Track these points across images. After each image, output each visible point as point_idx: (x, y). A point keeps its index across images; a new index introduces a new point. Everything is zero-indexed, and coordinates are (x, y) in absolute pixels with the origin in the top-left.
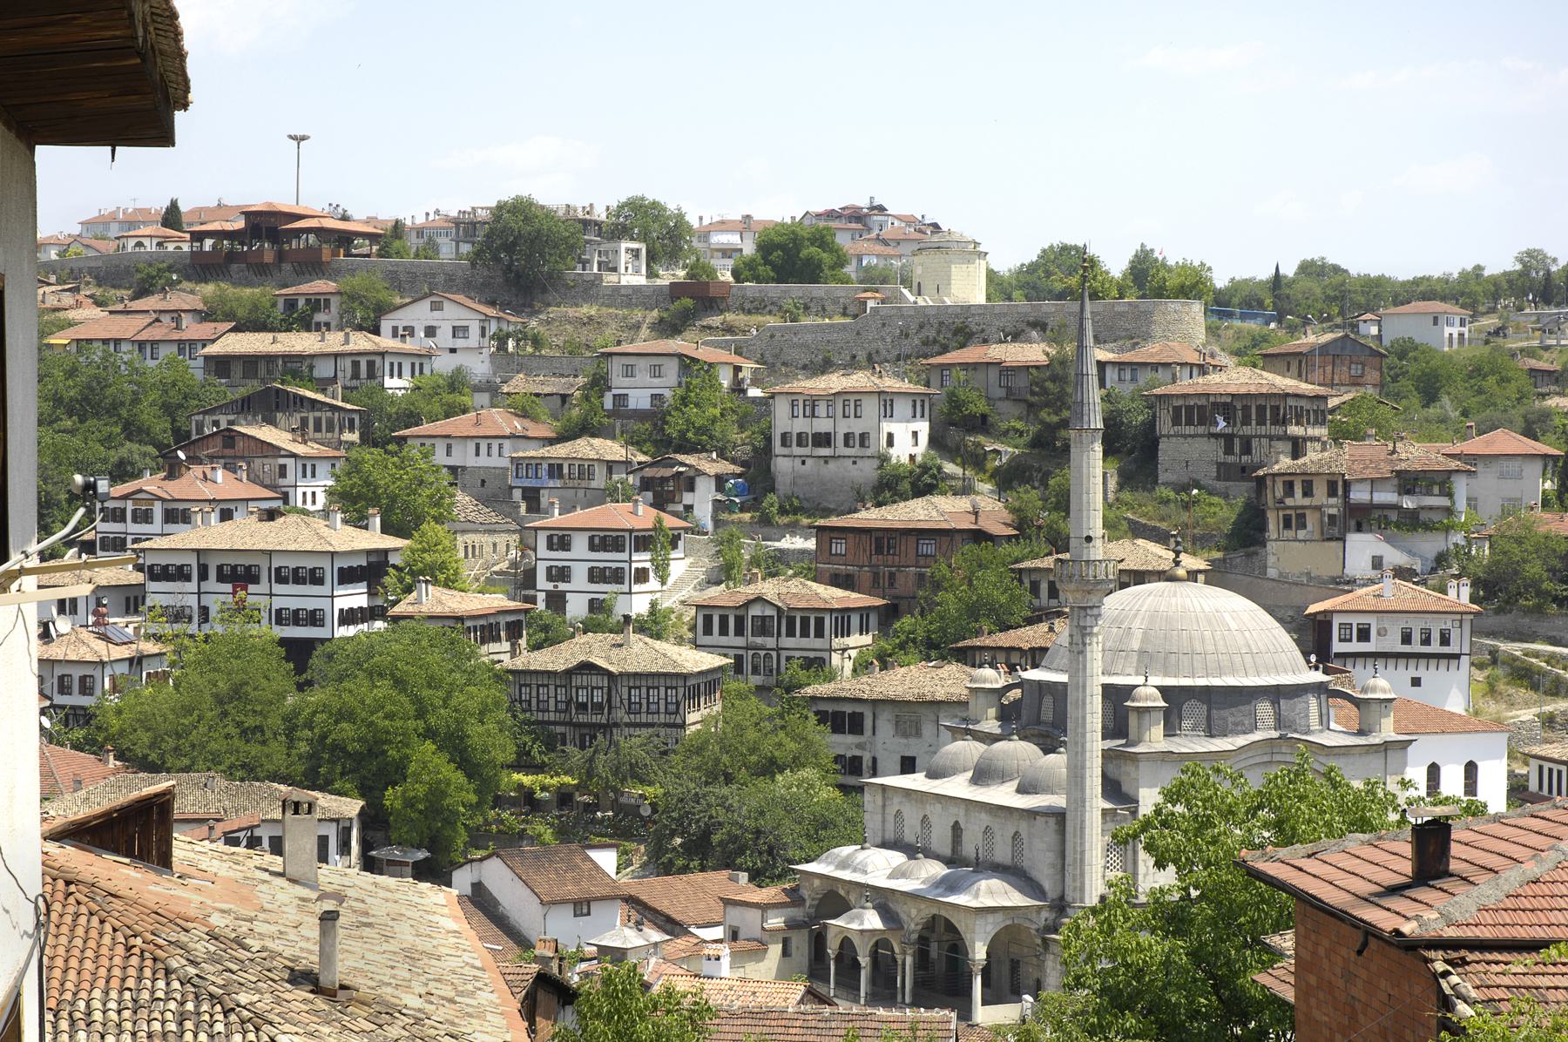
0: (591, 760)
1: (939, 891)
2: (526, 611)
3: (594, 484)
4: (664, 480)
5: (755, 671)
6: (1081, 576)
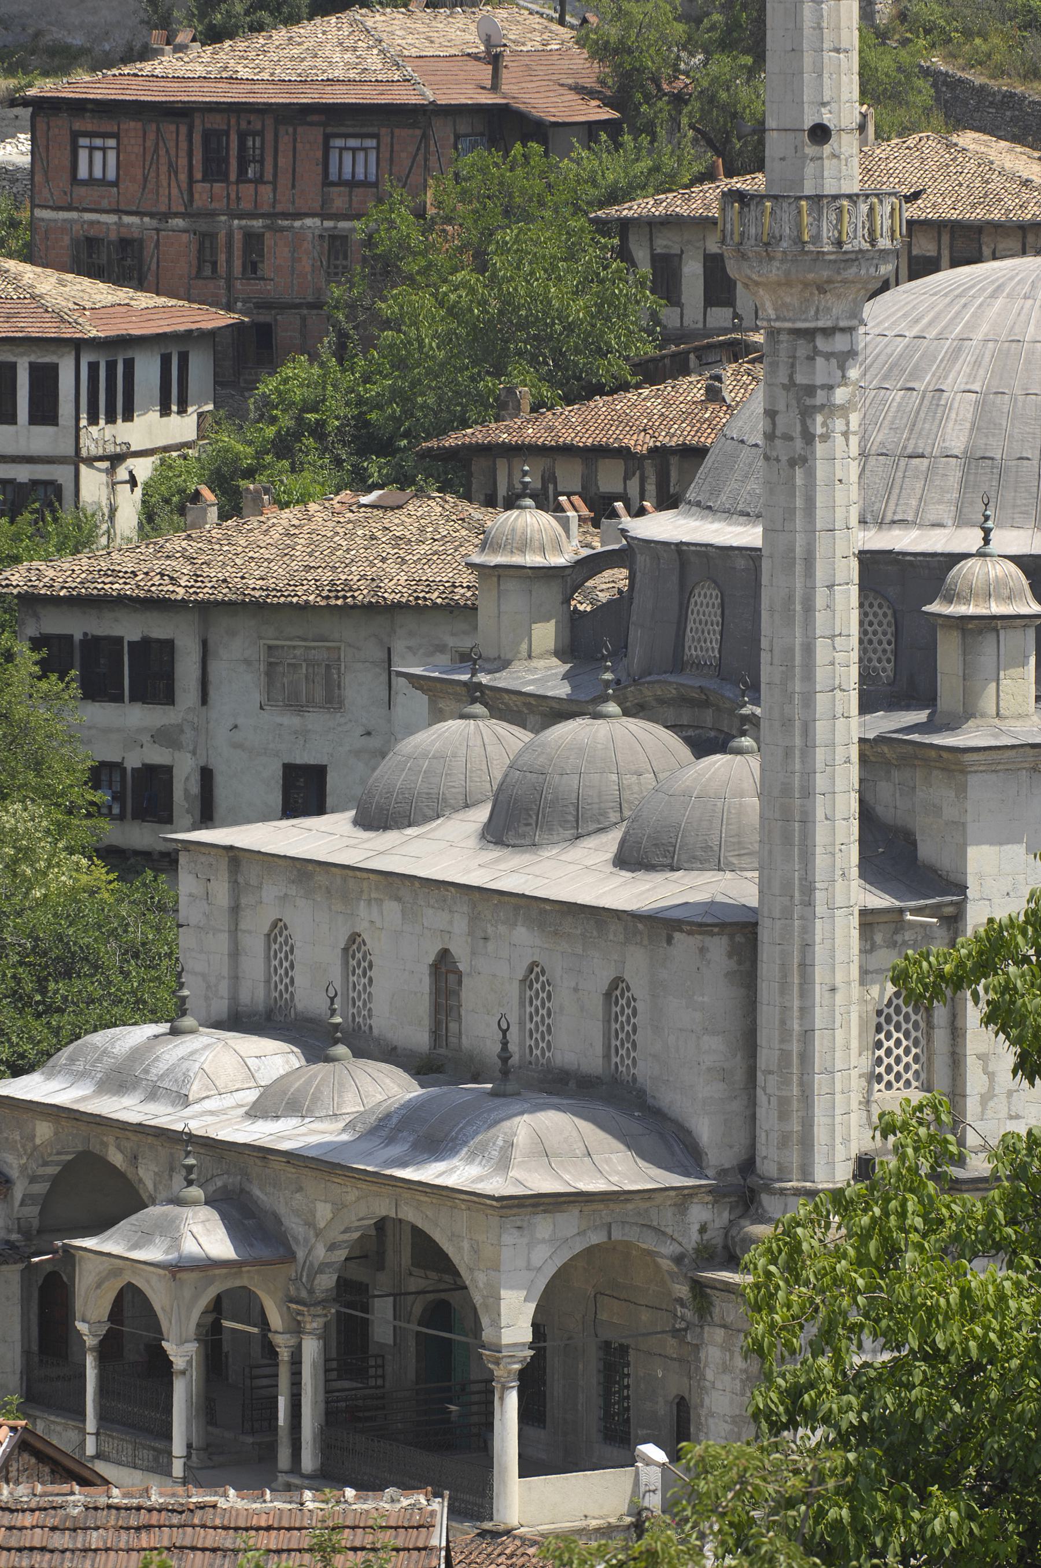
1: (396, 1150)
6: (799, 241)
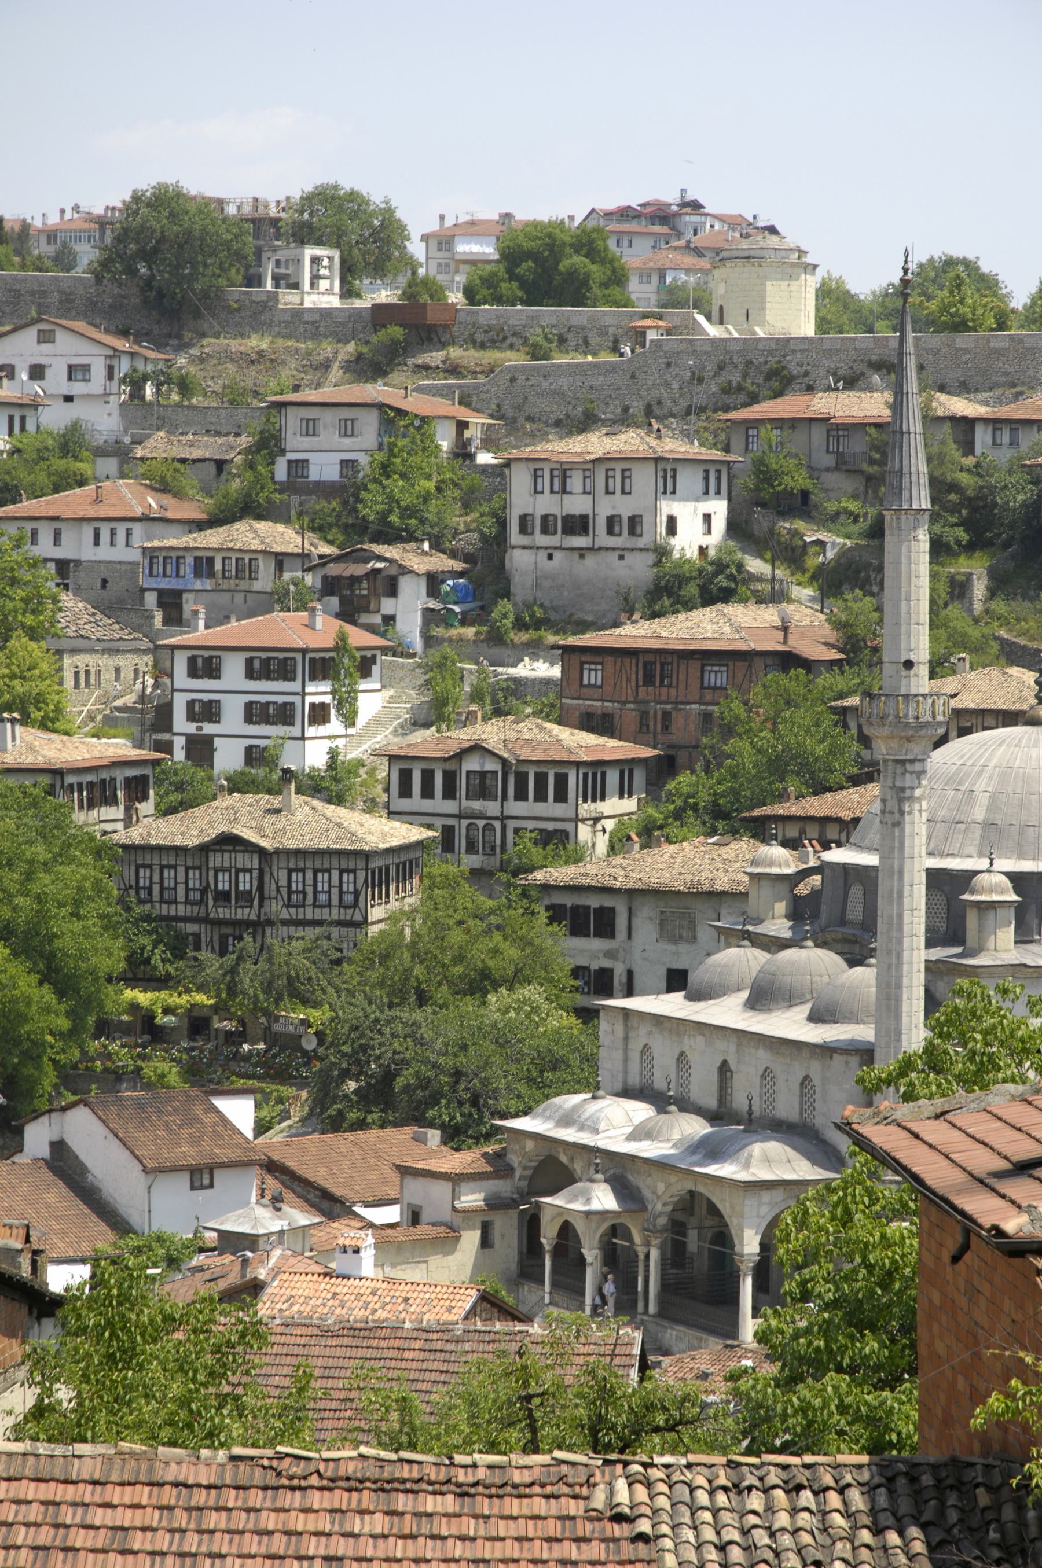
0: (233, 971)
1: (696, 1158)
2: (156, 763)
3: (257, 586)
4: (354, 580)
5: (471, 848)
6: (897, 716)
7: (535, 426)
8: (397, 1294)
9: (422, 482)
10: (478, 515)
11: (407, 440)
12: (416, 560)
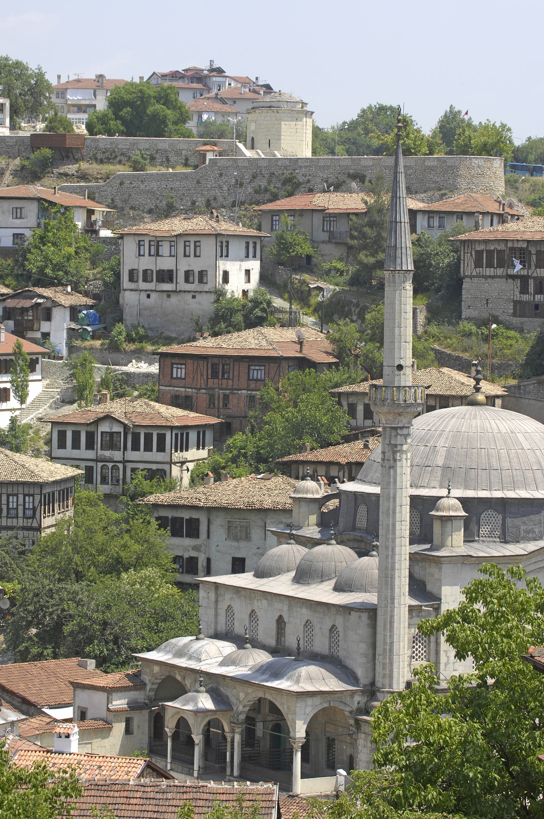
1: (265, 677)
4: (24, 310)
5: (104, 481)
6: (393, 400)
7: (136, 213)
8: (94, 763)
9: (67, 248)
10: (101, 269)
11: (56, 221)
12: (63, 298)
